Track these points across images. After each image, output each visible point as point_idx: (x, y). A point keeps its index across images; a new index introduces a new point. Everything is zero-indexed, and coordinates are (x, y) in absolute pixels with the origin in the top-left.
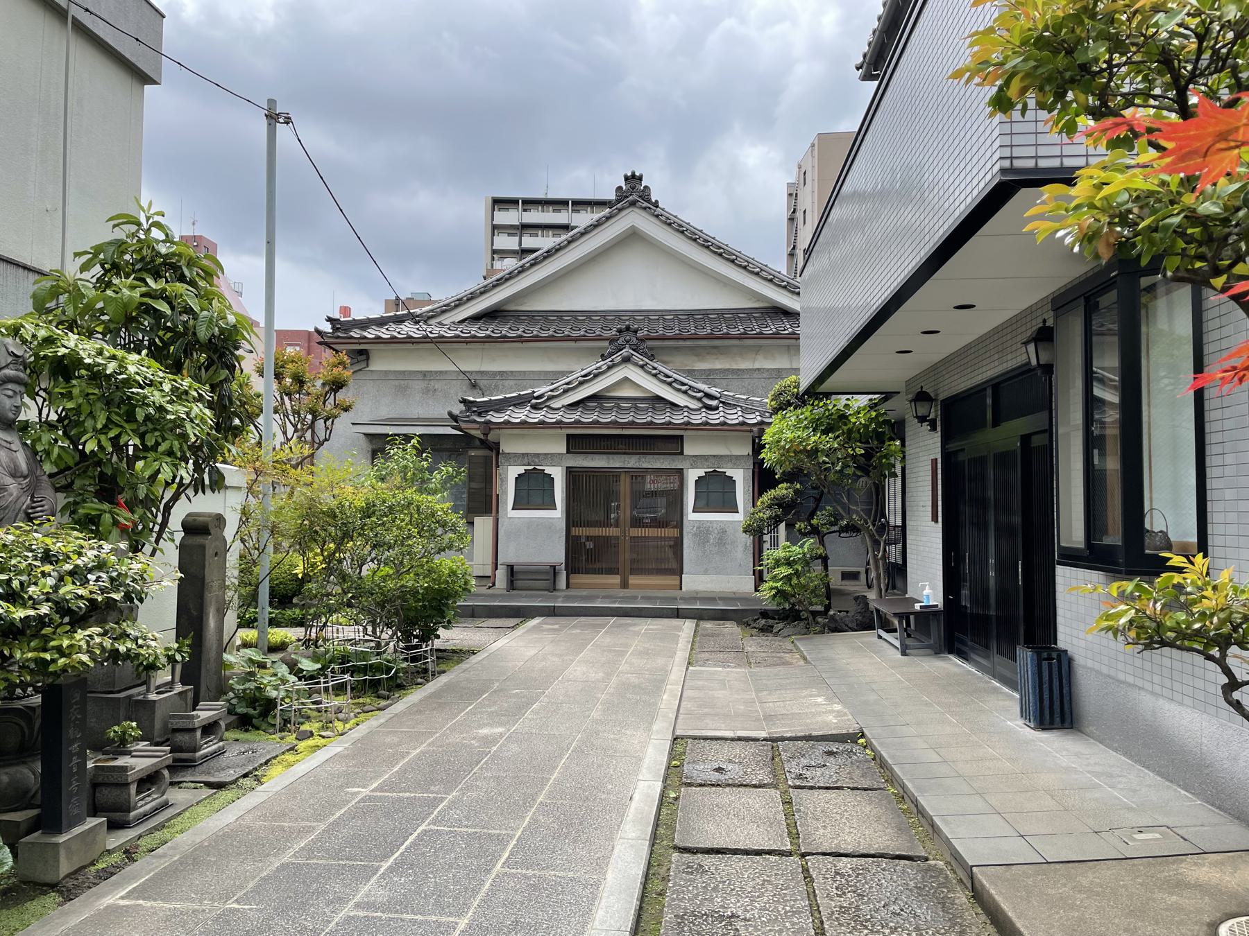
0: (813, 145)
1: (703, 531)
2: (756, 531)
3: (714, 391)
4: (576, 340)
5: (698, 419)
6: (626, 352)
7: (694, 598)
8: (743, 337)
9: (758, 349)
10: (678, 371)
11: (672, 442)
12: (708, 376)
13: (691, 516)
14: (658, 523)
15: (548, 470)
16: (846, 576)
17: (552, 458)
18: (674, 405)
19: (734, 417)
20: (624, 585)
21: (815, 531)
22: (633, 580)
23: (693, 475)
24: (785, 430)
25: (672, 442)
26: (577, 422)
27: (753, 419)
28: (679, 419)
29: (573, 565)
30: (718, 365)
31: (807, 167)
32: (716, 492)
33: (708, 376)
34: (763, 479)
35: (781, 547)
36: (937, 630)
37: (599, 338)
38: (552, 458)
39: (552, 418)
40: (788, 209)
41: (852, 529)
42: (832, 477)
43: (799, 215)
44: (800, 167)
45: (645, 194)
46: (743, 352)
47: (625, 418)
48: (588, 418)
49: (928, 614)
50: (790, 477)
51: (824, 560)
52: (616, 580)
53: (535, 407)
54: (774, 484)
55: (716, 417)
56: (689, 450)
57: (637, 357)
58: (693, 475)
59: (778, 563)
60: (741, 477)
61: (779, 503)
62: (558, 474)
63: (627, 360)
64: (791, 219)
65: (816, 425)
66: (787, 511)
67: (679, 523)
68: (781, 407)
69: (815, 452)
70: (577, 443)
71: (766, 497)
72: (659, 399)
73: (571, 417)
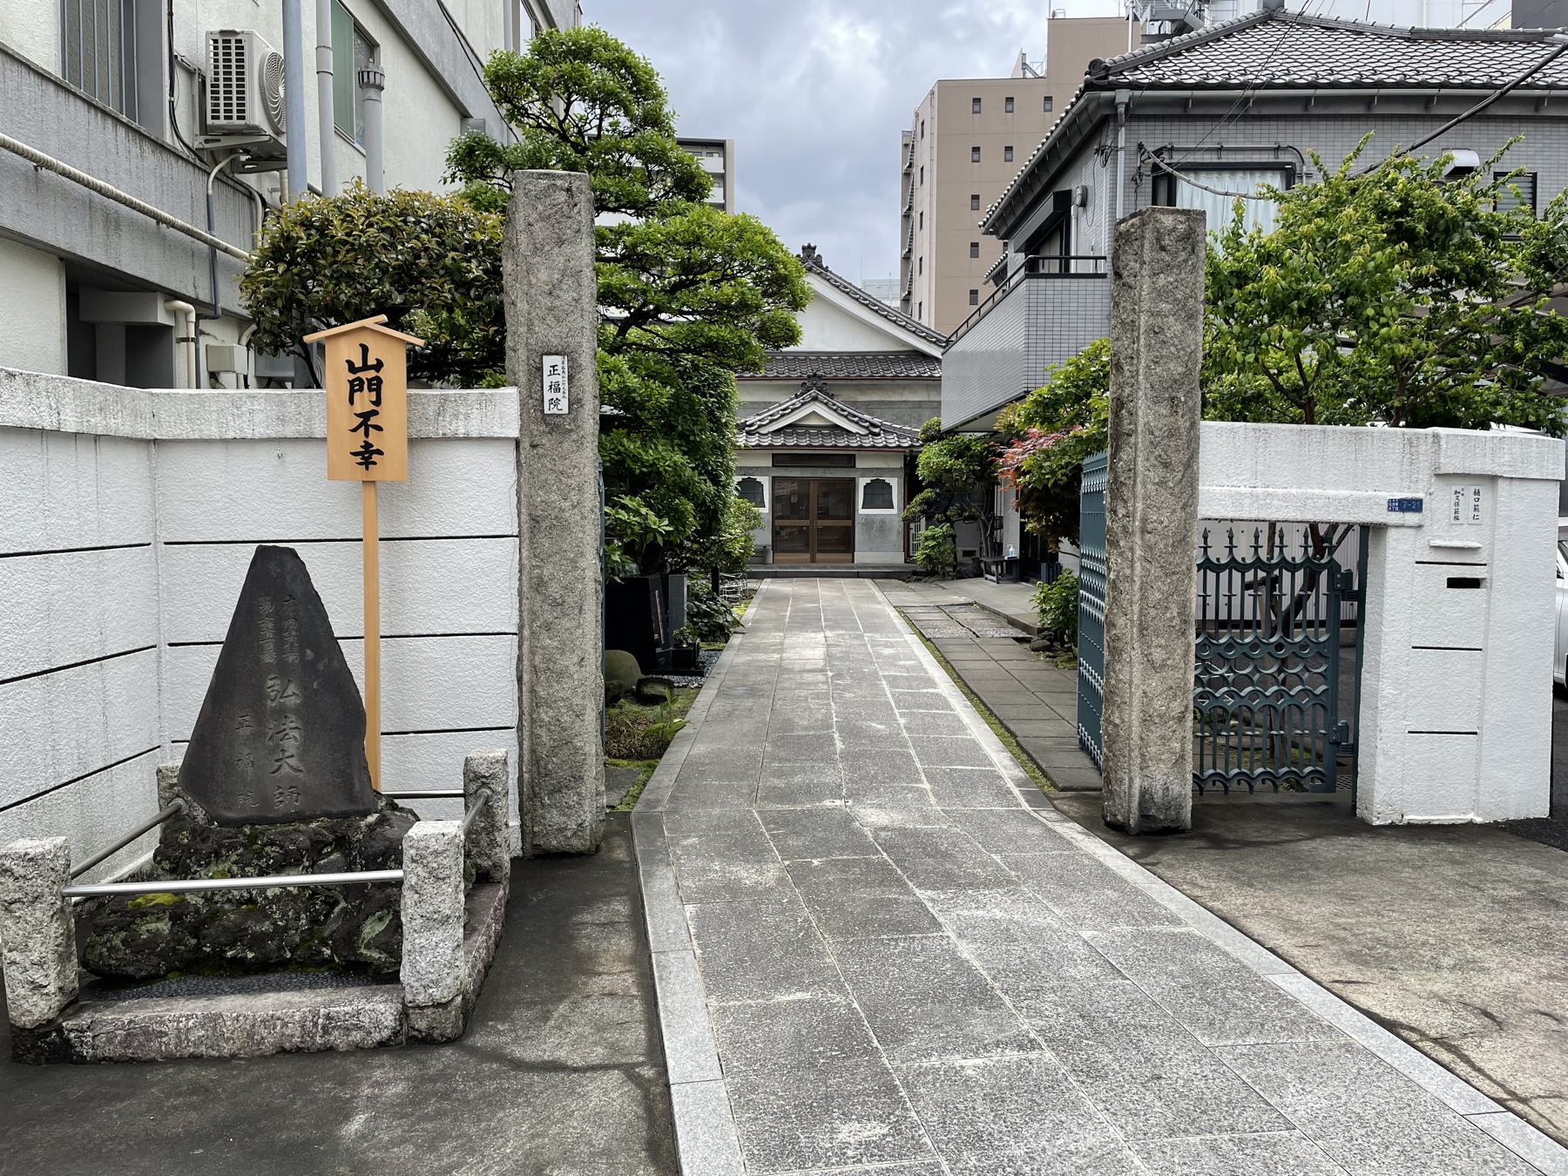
0: (932, 93)
1: (869, 521)
2: (907, 521)
3: (876, 421)
4: (771, 379)
5: (868, 442)
6: (813, 392)
7: (865, 566)
8: (895, 378)
9: (904, 387)
10: (845, 403)
11: (848, 460)
12: (869, 407)
13: (861, 511)
14: (782, 528)
15: (759, 479)
16: (966, 553)
17: (761, 470)
18: (848, 432)
19: (893, 441)
20: (813, 560)
21: (948, 519)
22: (819, 556)
23: (862, 482)
24: (931, 457)
25: (848, 460)
26: (796, 445)
27: (906, 443)
28: (854, 443)
29: (776, 547)
30: (875, 397)
31: (926, 116)
32: (877, 493)
33: (869, 407)
34: (912, 486)
35: (924, 531)
36: (1015, 571)
37: (788, 378)
38: (761, 470)
39: (766, 441)
40: (904, 163)
41: (972, 518)
42: (960, 484)
43: (916, 171)
44: (917, 116)
45: (818, 261)
46: (893, 389)
47: (817, 443)
48: (791, 442)
49: (1011, 561)
50: (930, 485)
51: (954, 537)
52: (807, 556)
53: (749, 433)
54: (921, 489)
55: (880, 441)
56: (859, 465)
57: (821, 396)
58: (862, 482)
59: (927, 539)
60: (895, 483)
61: (926, 502)
62: (765, 481)
63: (815, 399)
64: (907, 175)
65: (951, 454)
66: (931, 511)
67: (851, 514)
68: (929, 439)
69: (949, 471)
70: (781, 459)
71: (918, 498)
72: (836, 427)
73: (779, 441)
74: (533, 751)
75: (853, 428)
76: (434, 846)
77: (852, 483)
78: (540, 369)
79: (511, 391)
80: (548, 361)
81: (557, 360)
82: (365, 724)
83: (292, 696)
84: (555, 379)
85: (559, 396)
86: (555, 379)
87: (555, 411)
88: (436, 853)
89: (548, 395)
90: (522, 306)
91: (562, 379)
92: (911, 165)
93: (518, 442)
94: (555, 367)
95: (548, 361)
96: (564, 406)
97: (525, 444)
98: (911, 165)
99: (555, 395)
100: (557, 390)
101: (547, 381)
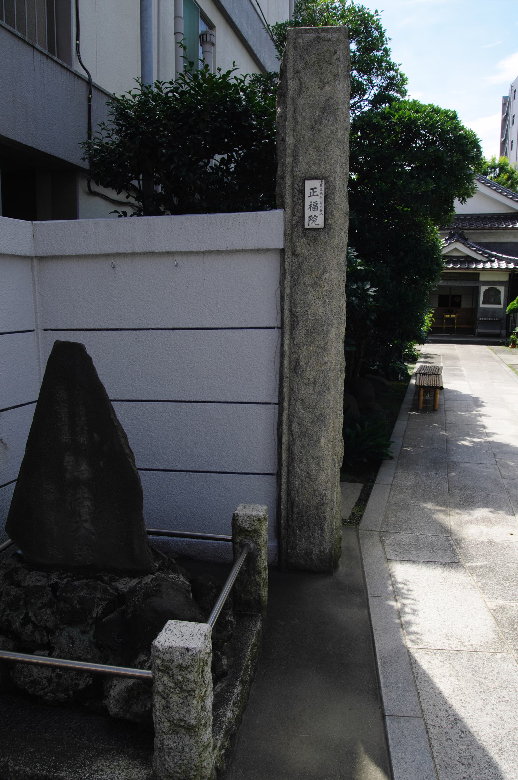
5: (488, 265)
13: (482, 306)
15: (498, 288)
23: (483, 289)
58: (483, 289)
72: (468, 257)
74: (289, 494)
75: (479, 258)
76: (178, 660)
77: (477, 290)
78: (302, 191)
79: (278, 214)
80: (309, 185)
81: (316, 184)
82: (142, 499)
83: (84, 470)
84: (314, 199)
85: (317, 213)
86: (314, 199)
87: (313, 225)
88: (181, 668)
89: (308, 213)
90: (290, 140)
91: (319, 199)
92: (507, 116)
93: (282, 251)
94: (314, 192)
95: (309, 185)
96: (320, 222)
97: (288, 254)
98: (507, 116)
99: (313, 213)
100: (316, 208)
101: (308, 201)
